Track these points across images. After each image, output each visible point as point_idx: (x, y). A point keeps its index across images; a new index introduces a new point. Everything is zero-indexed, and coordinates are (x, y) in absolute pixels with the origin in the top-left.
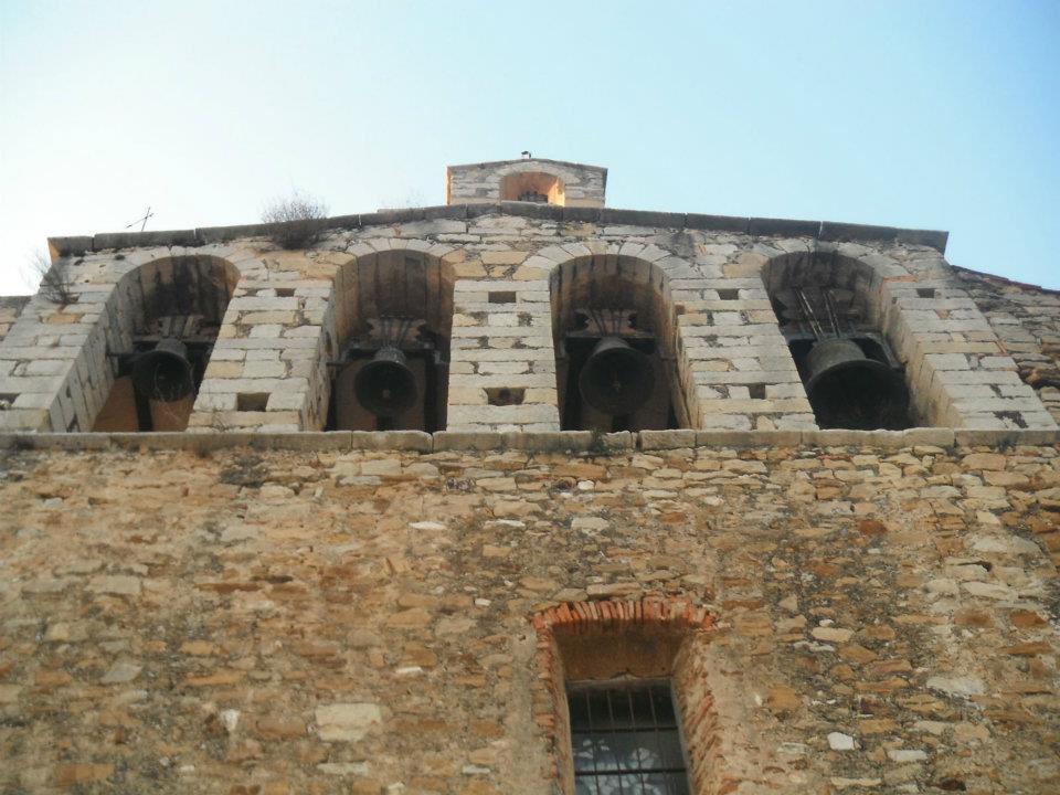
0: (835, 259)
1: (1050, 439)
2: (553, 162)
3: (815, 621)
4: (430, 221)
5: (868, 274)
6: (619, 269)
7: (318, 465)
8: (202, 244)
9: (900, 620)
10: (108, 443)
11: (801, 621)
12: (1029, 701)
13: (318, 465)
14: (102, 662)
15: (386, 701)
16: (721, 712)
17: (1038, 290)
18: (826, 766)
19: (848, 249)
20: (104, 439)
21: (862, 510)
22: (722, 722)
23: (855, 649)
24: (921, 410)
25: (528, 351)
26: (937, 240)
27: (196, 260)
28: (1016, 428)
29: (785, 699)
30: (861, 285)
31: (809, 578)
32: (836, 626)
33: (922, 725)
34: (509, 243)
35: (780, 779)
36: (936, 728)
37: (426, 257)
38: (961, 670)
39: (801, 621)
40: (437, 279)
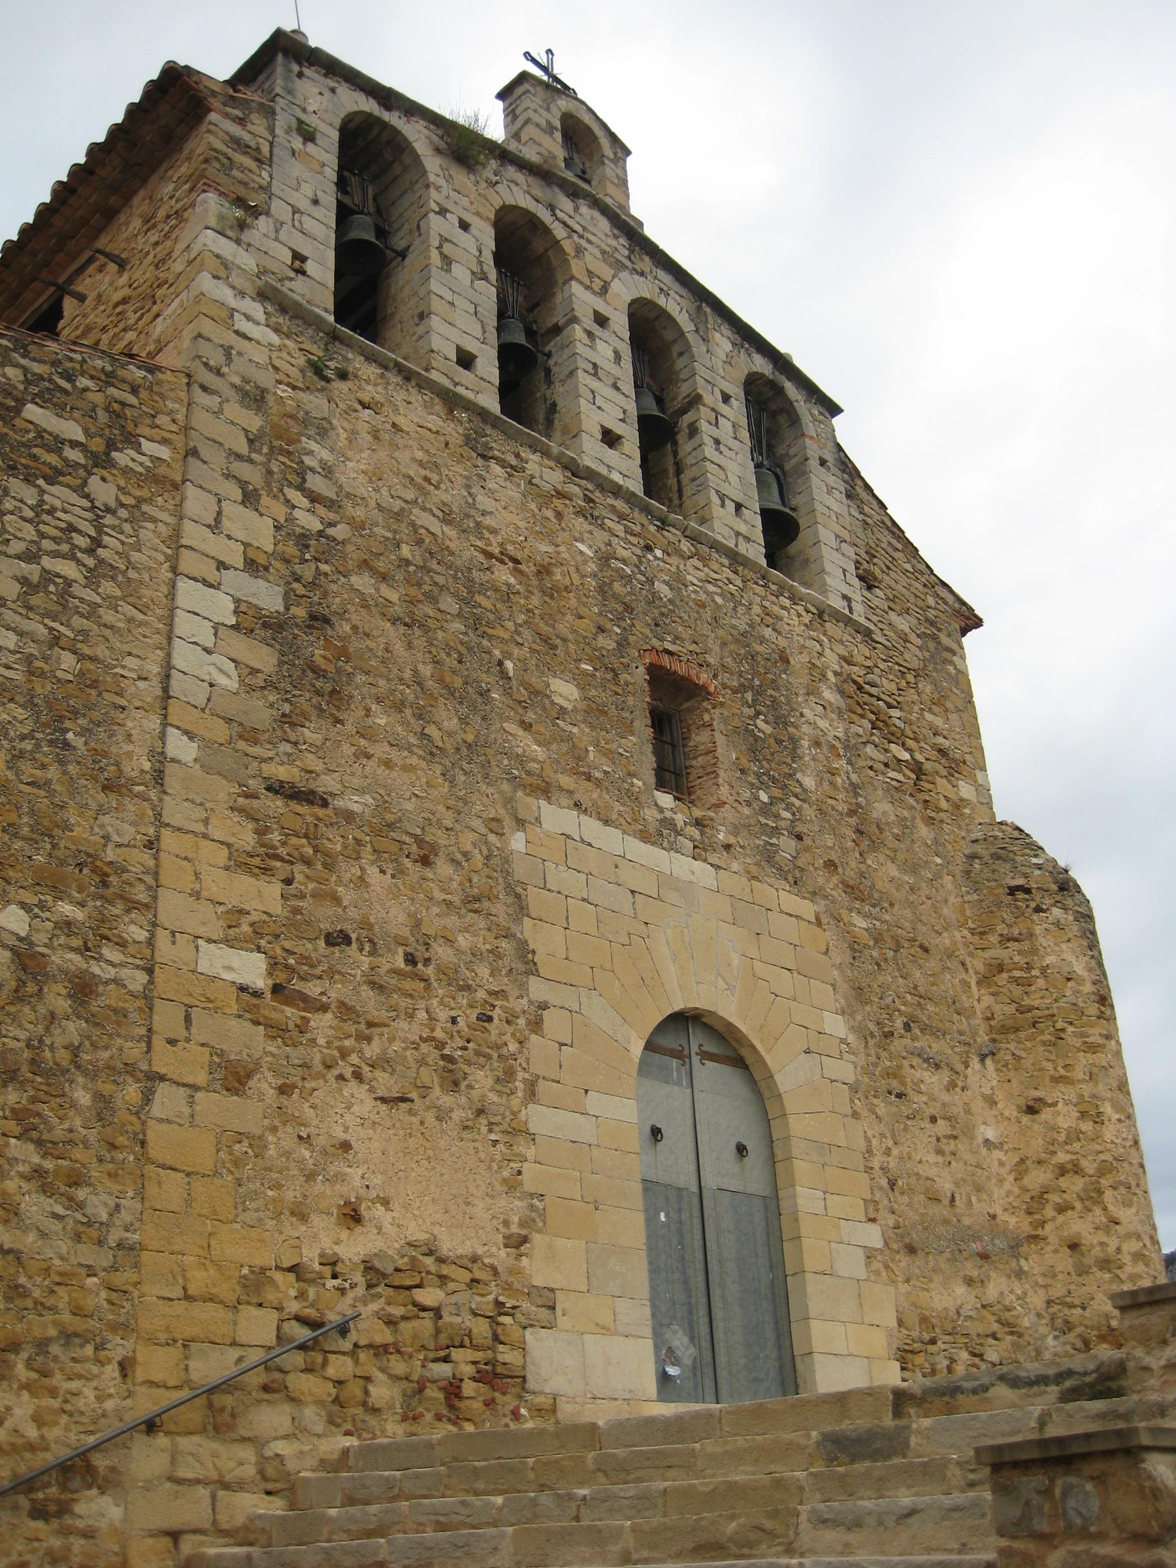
0: (780, 391)
1: (861, 629)
2: (597, 118)
3: (758, 714)
4: (549, 184)
5: (794, 420)
6: (657, 317)
7: (517, 455)
8: (388, 108)
9: (41, 527)
10: (392, 365)
11: (751, 712)
12: (830, 801)
13: (517, 455)
14: (436, 590)
15: (581, 688)
16: (721, 759)
17: (871, 490)
18: (757, 808)
19: (790, 388)
20: (391, 359)
21: (782, 643)
22: (720, 765)
23: (772, 740)
24: (791, 558)
25: (622, 397)
26: (834, 409)
27: (385, 125)
28: (847, 612)
29: (744, 762)
30: (782, 419)
31: (758, 683)
32: (766, 722)
33: (793, 799)
34: (603, 252)
35: (740, 808)
36: (797, 803)
37: (547, 231)
38: (809, 772)
39: (751, 712)
40: (542, 250)
